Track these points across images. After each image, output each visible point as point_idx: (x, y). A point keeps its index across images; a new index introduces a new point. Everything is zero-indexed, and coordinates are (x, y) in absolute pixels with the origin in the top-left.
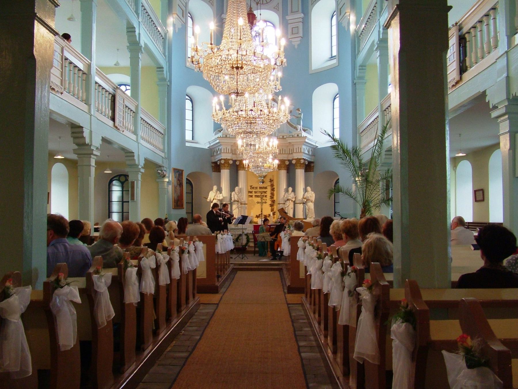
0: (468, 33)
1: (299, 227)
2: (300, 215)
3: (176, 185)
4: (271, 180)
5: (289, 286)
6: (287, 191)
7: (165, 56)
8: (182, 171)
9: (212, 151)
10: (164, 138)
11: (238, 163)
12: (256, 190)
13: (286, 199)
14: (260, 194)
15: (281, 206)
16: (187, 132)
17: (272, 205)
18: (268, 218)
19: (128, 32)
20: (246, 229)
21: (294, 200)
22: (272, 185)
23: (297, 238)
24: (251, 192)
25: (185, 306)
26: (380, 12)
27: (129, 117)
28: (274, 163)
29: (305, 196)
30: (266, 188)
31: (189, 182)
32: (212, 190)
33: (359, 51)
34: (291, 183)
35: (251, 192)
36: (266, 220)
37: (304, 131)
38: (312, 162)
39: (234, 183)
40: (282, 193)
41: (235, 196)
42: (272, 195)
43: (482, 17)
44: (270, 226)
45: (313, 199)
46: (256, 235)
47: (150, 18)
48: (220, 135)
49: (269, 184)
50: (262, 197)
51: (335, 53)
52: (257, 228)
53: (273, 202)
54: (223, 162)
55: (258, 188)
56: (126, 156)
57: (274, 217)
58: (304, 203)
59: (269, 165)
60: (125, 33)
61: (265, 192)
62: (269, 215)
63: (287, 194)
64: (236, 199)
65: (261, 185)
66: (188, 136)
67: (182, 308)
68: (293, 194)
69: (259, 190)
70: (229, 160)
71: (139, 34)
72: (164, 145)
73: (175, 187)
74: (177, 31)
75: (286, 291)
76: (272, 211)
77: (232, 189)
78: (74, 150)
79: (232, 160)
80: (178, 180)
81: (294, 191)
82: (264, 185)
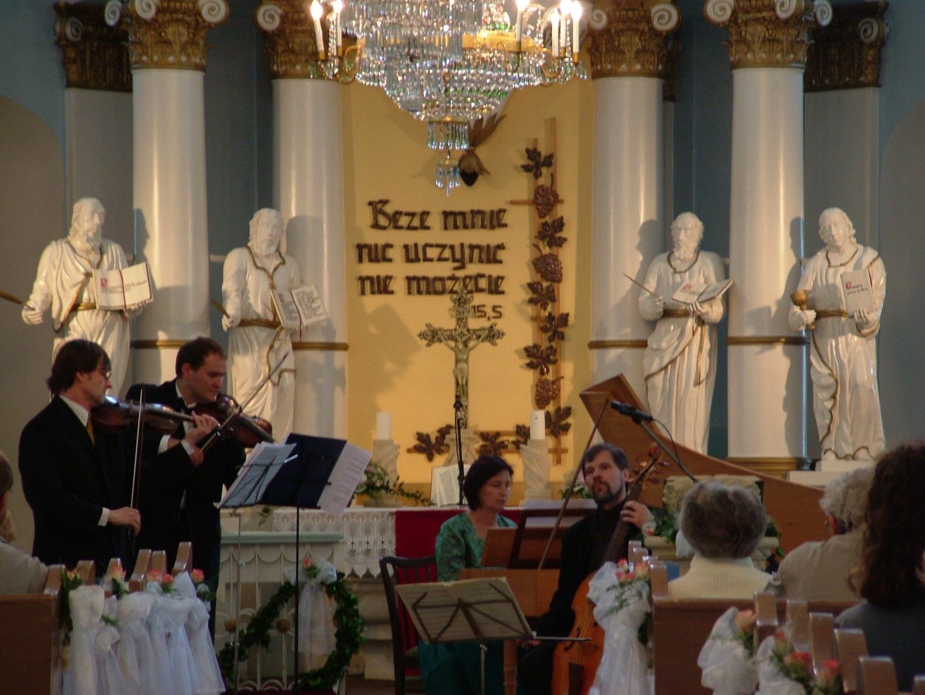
1: (725, 529)
2: (764, 433)
4: (532, 154)
6: (660, 241)
12: (420, 237)
13: (650, 308)
14: (444, 269)
15: (612, 363)
17: (539, 358)
18: (510, 458)
20: (329, 543)
21: (715, 311)
22: (545, 201)
23: (705, 613)
24: (378, 254)
28: (553, 17)
29: (807, 285)
30: (495, 220)
32: (61, 230)
34: (698, 178)
35: (378, 254)
36: (485, 473)
39: (241, 177)
40: (626, 257)
41: (247, 284)
42: (547, 271)
44: (520, 516)
45: (871, 302)
46: (407, 592)
50: (462, 293)
52: (418, 529)
53: (554, 327)
55: (435, 221)
57: (558, 453)
58: (794, 341)
59: (511, 37)
61: (491, 255)
62: (523, 433)
63: (660, 265)
64: (258, 308)
65: (456, 195)
68: (708, 266)
69: (437, 234)
76: (541, 401)
77: (225, 228)
81: (716, 241)
82: (480, 198)
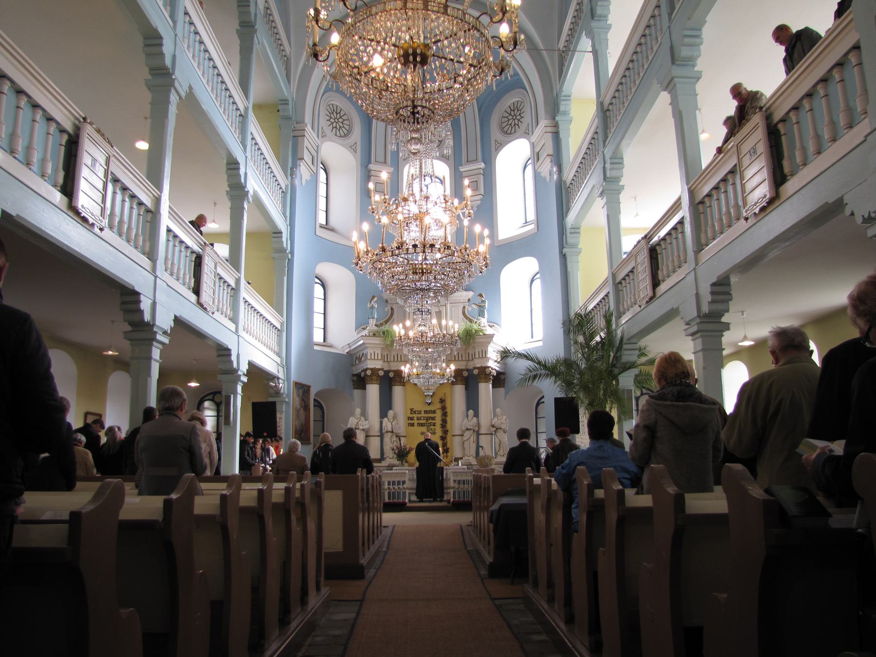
0: (783, 120)
3: (299, 407)
5: (491, 564)
7: (285, 217)
8: (309, 387)
9: (354, 357)
10: (280, 336)
11: (391, 375)
13: (464, 428)
14: (424, 421)
16: (316, 300)
19: (228, 169)
21: (477, 429)
22: (444, 408)
25: (299, 609)
26: (604, 142)
27: (225, 295)
30: (434, 412)
31: (318, 405)
33: (568, 209)
35: (412, 419)
37: (491, 327)
38: (503, 374)
39: (386, 404)
41: (387, 424)
43: (719, 183)
47: (262, 154)
48: (365, 332)
49: (439, 406)
51: (531, 216)
54: (369, 373)
56: (219, 356)
60: (225, 169)
61: (433, 419)
65: (428, 408)
66: (318, 337)
67: (293, 616)
68: (475, 419)
69: (423, 415)
70: (379, 369)
71: (246, 174)
72: (279, 344)
73: (297, 411)
74: (304, 184)
75: (484, 572)
77: (383, 414)
78: (125, 333)
79: (382, 369)
80: (303, 400)
